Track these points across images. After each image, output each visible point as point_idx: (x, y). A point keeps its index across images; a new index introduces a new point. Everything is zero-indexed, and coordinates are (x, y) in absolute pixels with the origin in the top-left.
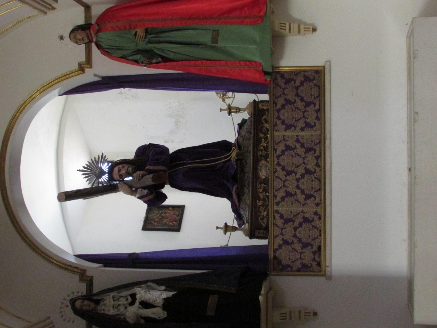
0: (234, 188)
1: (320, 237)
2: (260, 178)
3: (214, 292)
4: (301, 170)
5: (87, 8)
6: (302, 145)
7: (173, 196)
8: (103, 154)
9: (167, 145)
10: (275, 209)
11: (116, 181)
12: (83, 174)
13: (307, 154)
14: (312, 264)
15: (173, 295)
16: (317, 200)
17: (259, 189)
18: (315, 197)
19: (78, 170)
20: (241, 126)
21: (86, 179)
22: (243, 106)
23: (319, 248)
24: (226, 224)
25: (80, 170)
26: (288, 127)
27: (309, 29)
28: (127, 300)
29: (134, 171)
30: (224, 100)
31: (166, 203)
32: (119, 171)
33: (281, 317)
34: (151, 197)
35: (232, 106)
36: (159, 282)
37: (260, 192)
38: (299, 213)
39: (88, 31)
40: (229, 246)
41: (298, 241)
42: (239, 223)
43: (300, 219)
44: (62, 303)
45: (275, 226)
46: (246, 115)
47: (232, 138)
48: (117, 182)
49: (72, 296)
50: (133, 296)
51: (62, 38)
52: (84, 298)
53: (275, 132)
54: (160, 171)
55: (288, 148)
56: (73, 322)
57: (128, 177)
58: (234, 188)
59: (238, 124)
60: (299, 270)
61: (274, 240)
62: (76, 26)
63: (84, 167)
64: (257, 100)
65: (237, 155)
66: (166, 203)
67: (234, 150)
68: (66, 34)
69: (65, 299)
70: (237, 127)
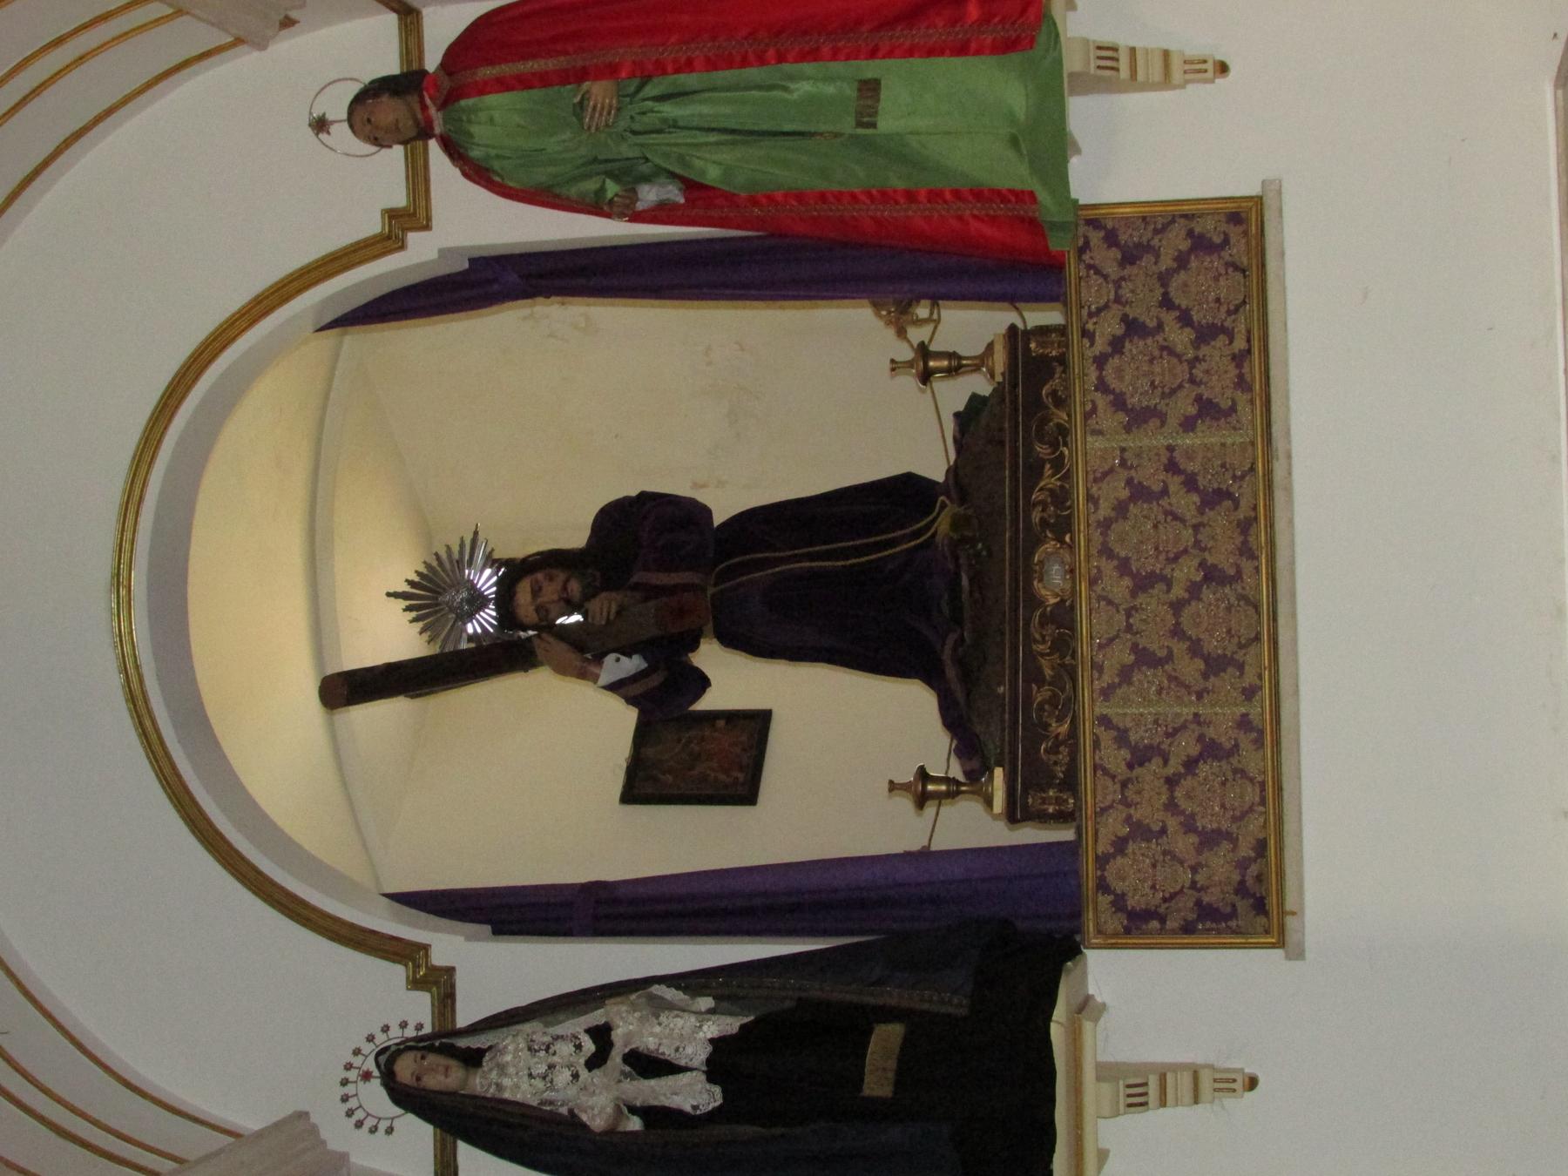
0: (951, 639)
1: (1261, 809)
2: (1040, 603)
3: (888, 1014)
4: (1187, 571)
5: (410, 19)
6: (1191, 483)
7: (732, 679)
8: (476, 533)
9: (703, 497)
10: (1098, 711)
11: (525, 630)
12: (408, 609)
13: (1212, 679)
14: (1234, 906)
15: (742, 1027)
16: (1250, 678)
17: (1036, 641)
18: (1241, 667)
19: (389, 595)
20: (967, 419)
21: (420, 624)
22: (970, 348)
23: (1261, 847)
24: (922, 768)
25: (396, 595)
26: (1138, 418)
27: (1203, 66)
28: (579, 1047)
29: (588, 595)
30: (901, 333)
31: (709, 702)
32: (536, 592)
33: (1129, 1096)
34: (656, 680)
35: (933, 348)
36: (691, 982)
37: (1043, 655)
38: (1184, 727)
39: (413, 100)
40: (934, 848)
41: (1189, 649)
42: (968, 768)
43: (1186, 745)
44: (348, 1067)
45: (1099, 773)
46: (980, 385)
47: (933, 463)
48: (531, 633)
49: (381, 1039)
50: (602, 1035)
51: (320, 125)
52: (422, 1045)
53: (1089, 439)
54: (686, 588)
55: (1139, 493)
56: (390, 1131)
57: (570, 614)
58: (951, 639)
59: (957, 415)
60: (1188, 929)
61: (1097, 823)
62: (372, 82)
63: (411, 583)
64: (1020, 326)
65: (956, 524)
66: (709, 702)
67: (943, 506)
68: (337, 105)
69: (357, 1052)
70: (950, 427)
